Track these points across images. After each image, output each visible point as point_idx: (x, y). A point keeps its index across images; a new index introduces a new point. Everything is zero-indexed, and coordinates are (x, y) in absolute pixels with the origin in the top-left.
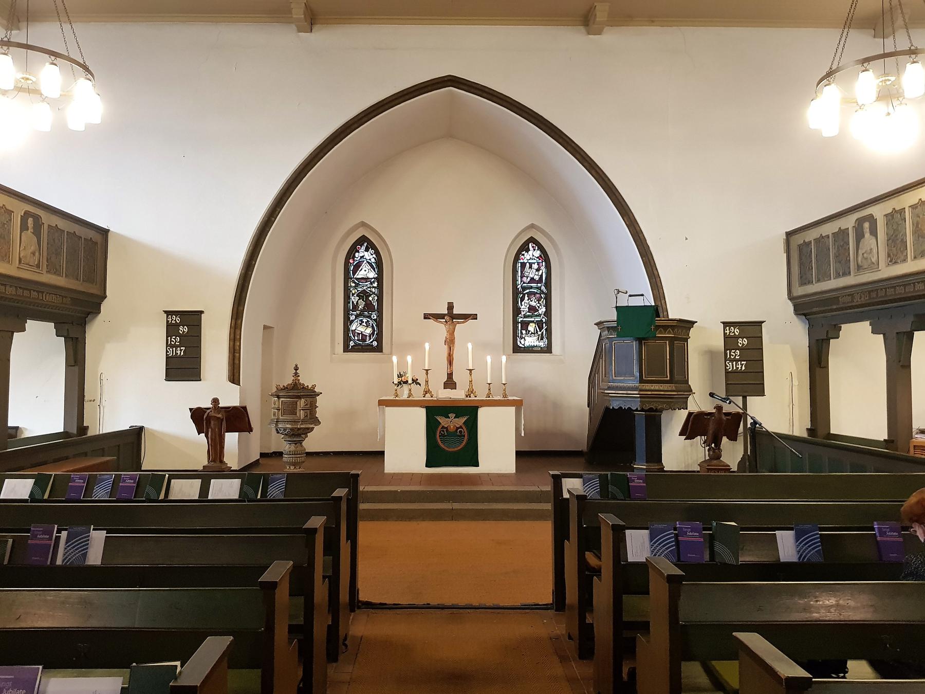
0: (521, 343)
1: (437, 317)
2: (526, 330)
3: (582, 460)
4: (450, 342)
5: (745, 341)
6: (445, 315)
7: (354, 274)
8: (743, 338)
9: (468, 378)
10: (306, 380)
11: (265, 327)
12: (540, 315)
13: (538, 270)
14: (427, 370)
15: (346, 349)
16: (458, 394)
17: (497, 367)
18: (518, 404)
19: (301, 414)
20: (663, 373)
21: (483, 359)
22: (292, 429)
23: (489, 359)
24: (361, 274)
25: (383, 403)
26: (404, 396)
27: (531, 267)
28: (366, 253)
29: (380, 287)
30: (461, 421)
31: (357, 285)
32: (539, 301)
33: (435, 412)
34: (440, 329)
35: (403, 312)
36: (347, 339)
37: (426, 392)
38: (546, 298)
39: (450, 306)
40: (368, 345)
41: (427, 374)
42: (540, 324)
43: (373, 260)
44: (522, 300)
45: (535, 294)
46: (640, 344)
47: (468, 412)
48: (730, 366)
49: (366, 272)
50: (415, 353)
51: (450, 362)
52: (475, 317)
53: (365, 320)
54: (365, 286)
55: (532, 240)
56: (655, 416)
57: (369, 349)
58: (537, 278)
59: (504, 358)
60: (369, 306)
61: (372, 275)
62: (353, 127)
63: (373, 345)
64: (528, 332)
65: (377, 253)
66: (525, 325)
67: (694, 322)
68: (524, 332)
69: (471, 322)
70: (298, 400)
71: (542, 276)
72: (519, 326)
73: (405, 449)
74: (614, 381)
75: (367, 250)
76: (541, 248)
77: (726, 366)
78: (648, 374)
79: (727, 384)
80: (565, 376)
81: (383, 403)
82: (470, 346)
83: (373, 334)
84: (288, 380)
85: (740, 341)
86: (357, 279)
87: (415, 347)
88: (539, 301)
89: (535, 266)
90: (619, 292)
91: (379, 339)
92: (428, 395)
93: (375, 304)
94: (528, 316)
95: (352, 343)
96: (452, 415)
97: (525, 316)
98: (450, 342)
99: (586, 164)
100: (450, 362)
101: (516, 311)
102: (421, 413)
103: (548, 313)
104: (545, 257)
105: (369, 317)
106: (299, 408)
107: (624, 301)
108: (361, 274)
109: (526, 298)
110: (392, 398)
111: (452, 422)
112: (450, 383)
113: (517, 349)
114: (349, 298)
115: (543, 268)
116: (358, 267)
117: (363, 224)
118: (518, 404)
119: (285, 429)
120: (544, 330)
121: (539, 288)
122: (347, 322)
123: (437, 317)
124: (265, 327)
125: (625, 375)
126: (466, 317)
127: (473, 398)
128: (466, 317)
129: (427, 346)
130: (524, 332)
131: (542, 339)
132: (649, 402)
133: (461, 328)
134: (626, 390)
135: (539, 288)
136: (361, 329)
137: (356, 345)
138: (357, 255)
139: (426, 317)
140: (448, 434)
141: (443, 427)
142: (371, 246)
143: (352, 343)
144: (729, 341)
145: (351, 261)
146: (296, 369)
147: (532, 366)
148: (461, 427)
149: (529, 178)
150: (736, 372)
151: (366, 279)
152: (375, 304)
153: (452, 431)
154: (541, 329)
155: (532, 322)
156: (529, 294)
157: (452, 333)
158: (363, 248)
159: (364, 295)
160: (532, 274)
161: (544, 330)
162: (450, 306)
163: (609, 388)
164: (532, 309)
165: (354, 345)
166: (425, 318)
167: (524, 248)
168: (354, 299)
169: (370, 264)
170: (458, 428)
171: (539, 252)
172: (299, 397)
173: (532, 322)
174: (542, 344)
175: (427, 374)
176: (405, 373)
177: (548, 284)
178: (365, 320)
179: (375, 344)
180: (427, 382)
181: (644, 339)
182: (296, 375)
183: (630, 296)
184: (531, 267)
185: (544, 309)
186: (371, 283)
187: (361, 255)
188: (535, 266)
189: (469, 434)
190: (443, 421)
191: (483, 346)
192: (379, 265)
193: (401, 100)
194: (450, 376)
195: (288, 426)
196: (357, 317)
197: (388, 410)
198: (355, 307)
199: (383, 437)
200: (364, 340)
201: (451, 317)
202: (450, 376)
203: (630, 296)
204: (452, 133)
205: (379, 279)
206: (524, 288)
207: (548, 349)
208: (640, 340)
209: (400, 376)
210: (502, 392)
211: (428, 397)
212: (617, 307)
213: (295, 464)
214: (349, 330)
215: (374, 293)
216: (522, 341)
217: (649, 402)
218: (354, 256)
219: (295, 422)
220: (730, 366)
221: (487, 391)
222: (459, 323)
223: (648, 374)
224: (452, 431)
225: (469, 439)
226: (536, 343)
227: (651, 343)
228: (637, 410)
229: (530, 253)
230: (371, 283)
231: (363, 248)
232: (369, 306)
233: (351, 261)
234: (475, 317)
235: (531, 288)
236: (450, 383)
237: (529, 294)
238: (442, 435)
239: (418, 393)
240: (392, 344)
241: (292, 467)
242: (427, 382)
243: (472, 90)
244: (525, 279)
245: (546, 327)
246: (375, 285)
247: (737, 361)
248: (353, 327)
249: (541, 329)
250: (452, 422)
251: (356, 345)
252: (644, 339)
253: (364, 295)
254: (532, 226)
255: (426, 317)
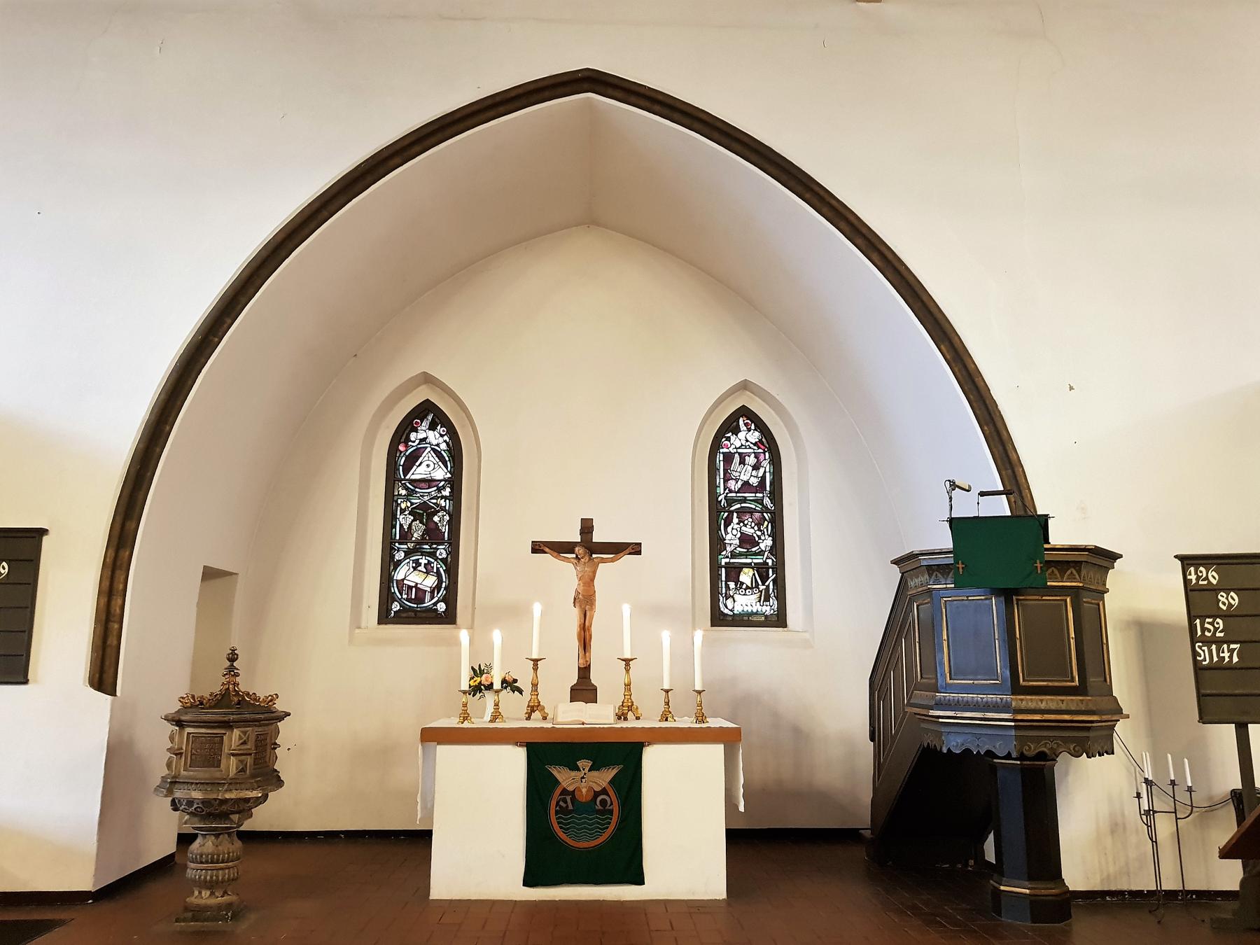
0: (727, 607)
1: (561, 548)
2: (737, 581)
3: (860, 853)
4: (585, 600)
5: (1234, 599)
6: (574, 544)
7: (406, 472)
8: (1227, 591)
9: (622, 677)
10: (255, 684)
11: (210, 574)
12: (761, 553)
13: (756, 467)
14: (536, 661)
15: (385, 617)
16: (598, 716)
17: (683, 658)
18: (729, 738)
19: (231, 766)
20: (1066, 672)
21: (655, 641)
22: (205, 802)
23: (666, 636)
24: (419, 472)
25: (433, 736)
26: (482, 720)
27: (742, 462)
28: (431, 434)
29: (456, 497)
30: (603, 778)
31: (411, 493)
32: (759, 524)
33: (547, 755)
34: (565, 573)
35: (494, 544)
36: (386, 597)
37: (533, 708)
38: (772, 521)
39: (587, 527)
40: (428, 610)
41: (535, 668)
42: (762, 570)
43: (444, 446)
44: (728, 522)
45: (751, 512)
46: (1009, 604)
47: (622, 756)
48: (1204, 655)
49: (429, 468)
50: (517, 621)
51: (585, 644)
52: (636, 549)
53: (423, 561)
54: (425, 495)
55: (744, 412)
56: (1042, 768)
57: (431, 617)
58: (754, 481)
59: (699, 635)
60: (432, 534)
61: (440, 474)
62: (392, 163)
63: (438, 610)
64: (739, 584)
65: (452, 432)
66: (734, 572)
67: (1121, 556)
68: (732, 585)
69: (627, 559)
70: (232, 727)
71: (764, 477)
72: (723, 574)
73: (480, 844)
74: (947, 688)
75: (432, 427)
76: (761, 426)
77: (1195, 654)
78: (1030, 674)
79: (1200, 696)
80: (821, 669)
81: (433, 736)
82: (626, 609)
83: (438, 587)
84: (213, 685)
85: (1222, 597)
86: (411, 481)
87: (514, 613)
88: (759, 524)
89: (751, 460)
90: (954, 485)
91: (451, 598)
92: (537, 715)
93: (445, 529)
94: (741, 555)
95: (396, 607)
96: (584, 764)
97: (733, 555)
98: (585, 600)
99: (859, 241)
100: (585, 644)
101: (717, 544)
102: (515, 760)
103: (778, 548)
104: (769, 443)
105: (433, 555)
106: (226, 750)
107: (967, 507)
108: (419, 472)
109: (735, 520)
110: (453, 722)
111: (584, 781)
112: (584, 690)
113: (719, 619)
114: (394, 517)
115: (765, 464)
116: (413, 459)
117: (427, 379)
118: (729, 738)
119: (190, 802)
120: (770, 582)
121: (760, 501)
122: (389, 564)
123: (561, 548)
124: (210, 574)
125: (974, 674)
126: (617, 549)
127: (631, 723)
128: (617, 549)
129: (537, 608)
130: (732, 585)
131: (767, 599)
132: (1037, 740)
133: (608, 572)
134: (974, 711)
135: (760, 501)
136: (415, 578)
137: (404, 609)
138: (413, 436)
139: (537, 548)
140: (575, 807)
141: (565, 792)
142: (439, 419)
143: (396, 607)
144: (1198, 600)
145: (401, 448)
146: (233, 657)
147: (751, 653)
148: (604, 791)
149: (737, 290)
150: (1219, 667)
151: (429, 482)
152: (445, 529)
153: (583, 802)
154: (764, 579)
155: (748, 565)
156: (740, 512)
157: (588, 582)
158: (425, 424)
159: (424, 513)
160: (746, 474)
161: (770, 582)
162: (587, 527)
163: (940, 705)
164: (746, 540)
165: (400, 609)
166: (534, 551)
167: (730, 426)
168: (404, 520)
169: (438, 454)
170: (597, 794)
171: (757, 434)
172: (228, 725)
173: (748, 565)
174: (767, 609)
175: (535, 668)
176: (490, 667)
177: (776, 494)
178: (423, 561)
179: (442, 607)
180: (535, 686)
181: (1017, 591)
182: (232, 671)
183: (982, 494)
184: (742, 462)
185: (769, 542)
186: (439, 490)
187: (422, 435)
188: (751, 460)
189: (623, 805)
190: (565, 778)
191: (657, 612)
192: (454, 456)
193: (492, 113)
194: (584, 672)
195: (197, 795)
196: (408, 553)
197: (445, 753)
198: (406, 535)
199: (429, 813)
200: (420, 598)
201: (588, 548)
202: (584, 672)
203: (982, 494)
204: (596, 210)
205: (455, 482)
206: (730, 502)
207: (779, 620)
208: (1007, 595)
209: (478, 672)
210: (694, 709)
211: (536, 723)
212: (952, 522)
213: (211, 886)
214: (390, 579)
215: (443, 509)
216: (729, 603)
217: (1037, 740)
218: (408, 439)
219: (214, 784)
220: (1204, 655)
221: (662, 707)
222: (604, 561)
223: (1030, 674)
224: (583, 802)
225: (619, 829)
226: (757, 608)
227: (1032, 600)
228: (1008, 756)
229: (742, 435)
230: (439, 490)
231: (425, 424)
232: (432, 534)
233: (401, 448)
234: (636, 549)
235: (745, 500)
236: (584, 690)
237: (740, 512)
238: (562, 811)
239: (514, 713)
240: (474, 608)
241: (206, 893)
242: (535, 686)
243: (633, 99)
244: (732, 484)
245: (772, 575)
246: (447, 492)
247: (1218, 642)
248: (399, 574)
249: (764, 579)
250: (584, 781)
251: (404, 609)
252: (1017, 591)
253: (424, 513)
254: (745, 386)
255: (537, 548)
